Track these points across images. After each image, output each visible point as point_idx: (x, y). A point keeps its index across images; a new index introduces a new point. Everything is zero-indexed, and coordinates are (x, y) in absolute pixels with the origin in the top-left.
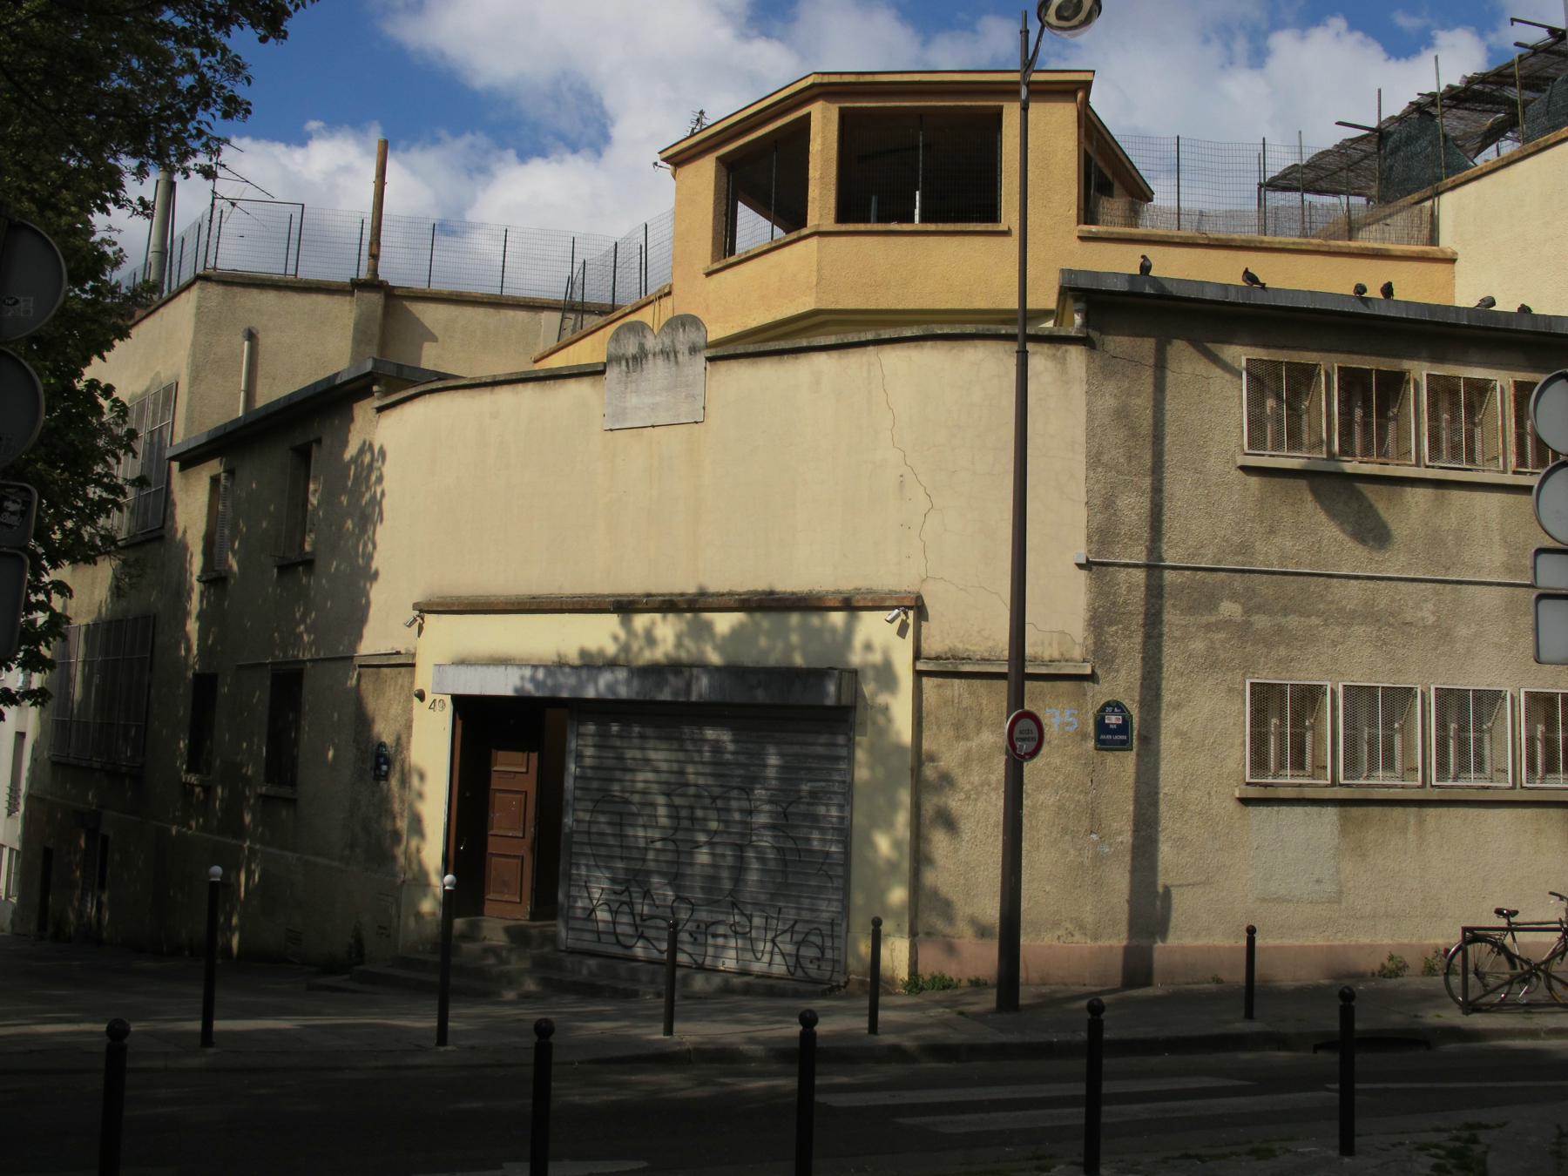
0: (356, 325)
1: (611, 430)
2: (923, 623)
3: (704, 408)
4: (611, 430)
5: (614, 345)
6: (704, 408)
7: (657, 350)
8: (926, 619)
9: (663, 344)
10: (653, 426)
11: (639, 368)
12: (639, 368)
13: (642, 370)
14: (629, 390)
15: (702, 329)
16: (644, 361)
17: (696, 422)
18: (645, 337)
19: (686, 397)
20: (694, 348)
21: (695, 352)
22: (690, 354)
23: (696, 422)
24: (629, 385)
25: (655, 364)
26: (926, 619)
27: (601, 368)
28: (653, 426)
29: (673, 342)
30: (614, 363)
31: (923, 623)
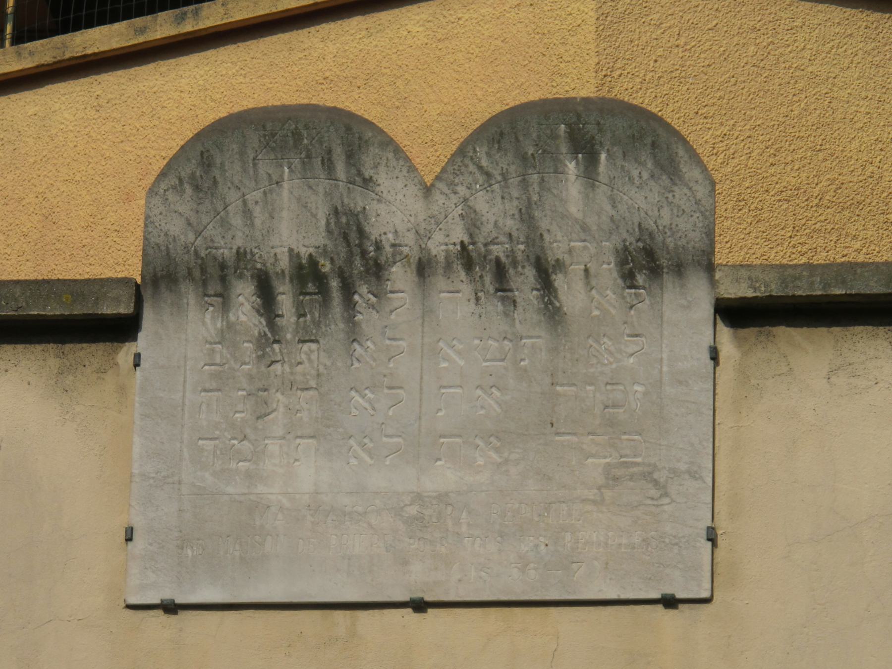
0: (79, 343)
1: (170, 608)
2: (712, 344)
3: (712, 538)
4: (170, 608)
5: (185, 204)
6: (712, 538)
7: (437, 246)
8: (710, 347)
9: (472, 221)
10: (420, 606)
11: (337, 326)
12: (337, 326)
13: (354, 334)
14: (278, 421)
15: (691, 173)
16: (363, 294)
17: (670, 602)
18: (367, 183)
19: (612, 479)
20: (650, 253)
21: (655, 271)
22: (628, 278)
23: (670, 602)
24: (279, 399)
25: (427, 313)
26: (710, 347)
27: (125, 308)
28: (420, 606)
29: (527, 216)
30: (190, 295)
31: (712, 344)
